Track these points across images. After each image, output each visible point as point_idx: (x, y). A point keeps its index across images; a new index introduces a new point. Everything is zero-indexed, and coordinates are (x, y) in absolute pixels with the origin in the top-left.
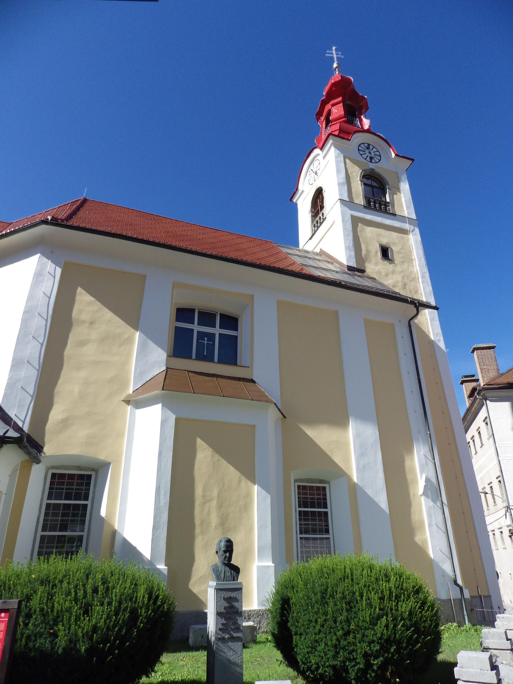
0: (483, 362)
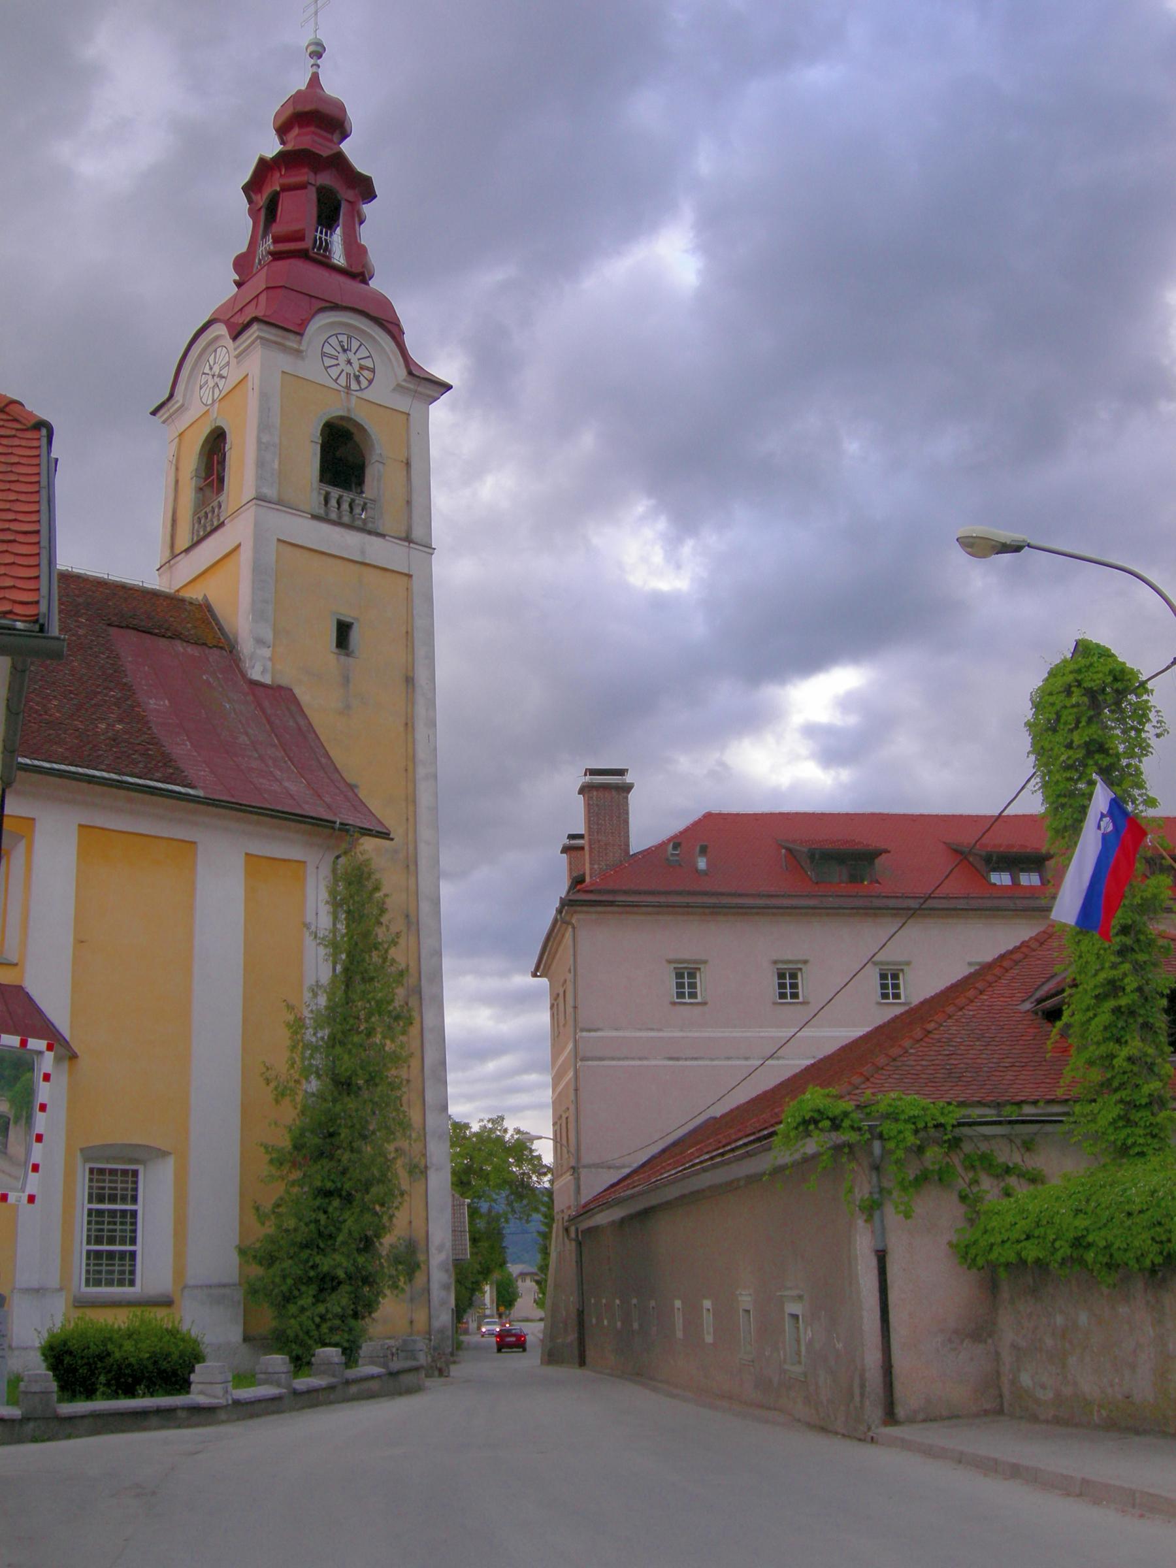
0: (598, 824)
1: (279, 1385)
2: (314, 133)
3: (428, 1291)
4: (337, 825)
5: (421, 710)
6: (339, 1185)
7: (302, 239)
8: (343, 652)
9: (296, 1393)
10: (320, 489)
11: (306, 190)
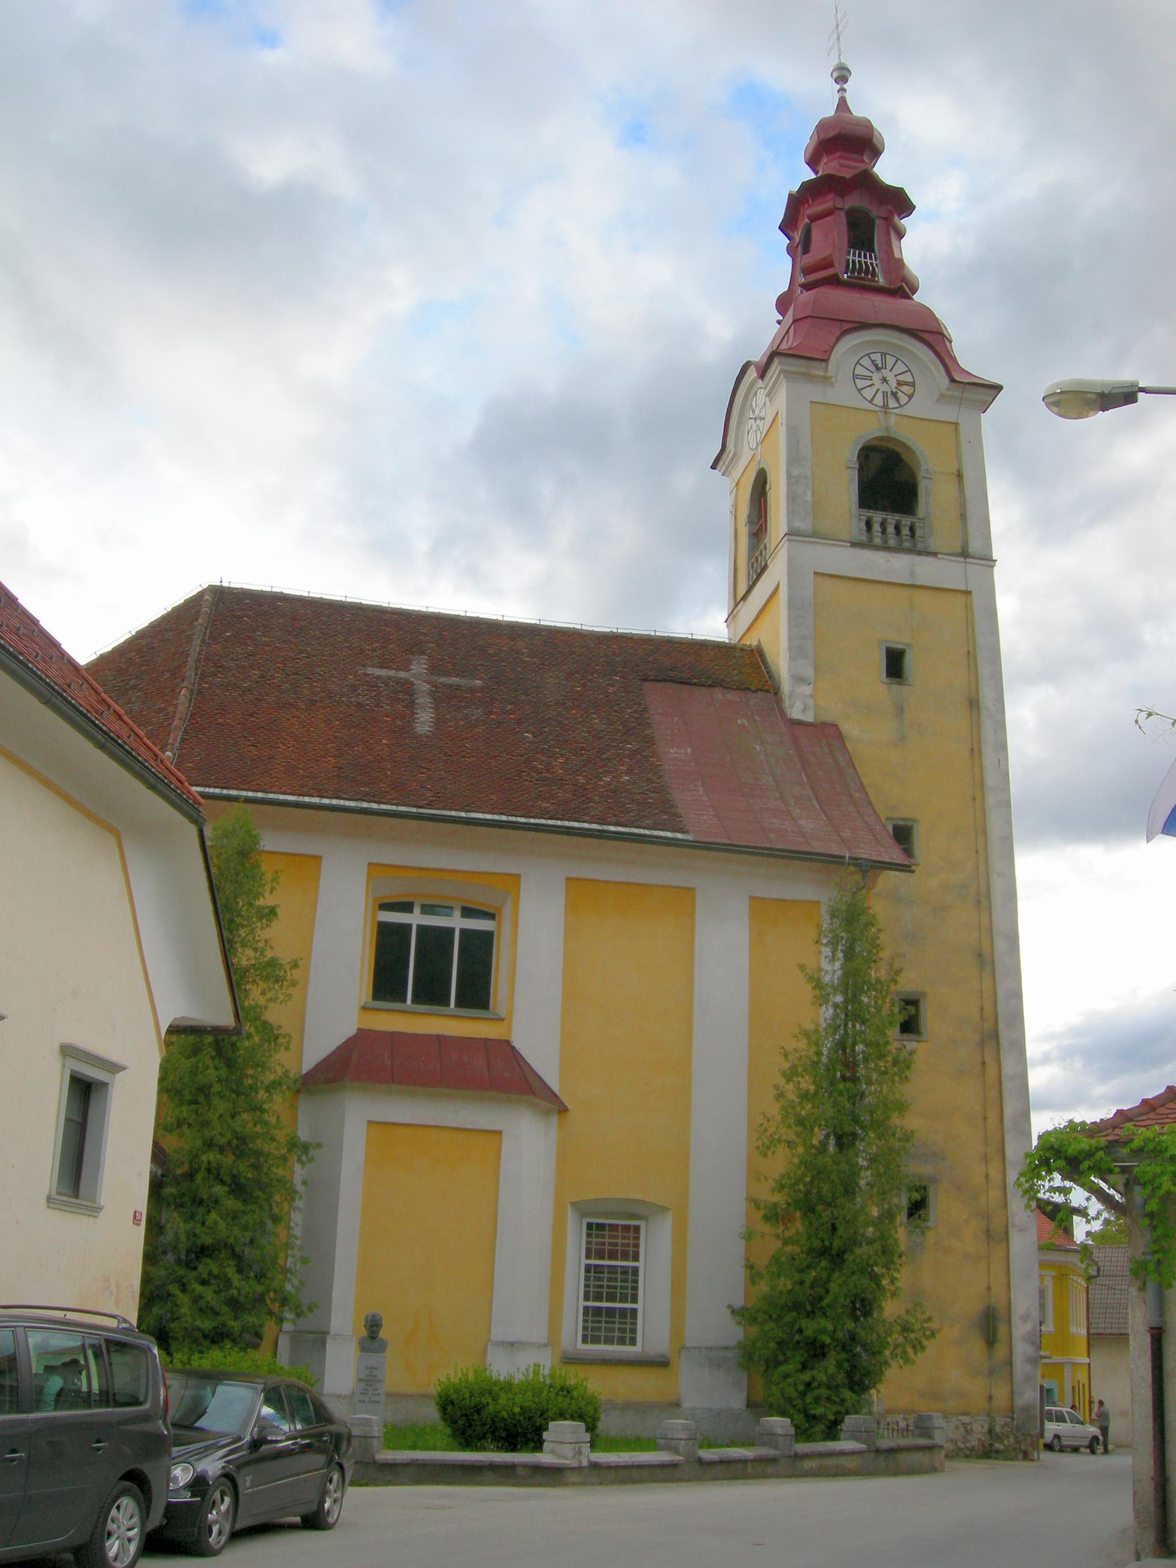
1: (677, 1452)
2: (841, 157)
3: (1010, 1364)
4: (847, 860)
5: (988, 734)
6: (827, 1243)
7: (831, 265)
8: (895, 680)
9: (701, 1461)
10: (860, 515)
11: (833, 216)
